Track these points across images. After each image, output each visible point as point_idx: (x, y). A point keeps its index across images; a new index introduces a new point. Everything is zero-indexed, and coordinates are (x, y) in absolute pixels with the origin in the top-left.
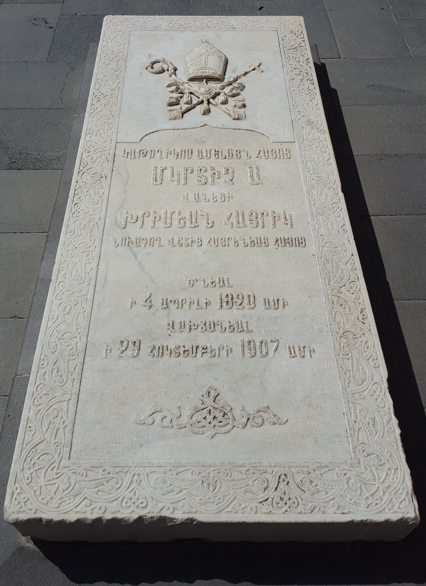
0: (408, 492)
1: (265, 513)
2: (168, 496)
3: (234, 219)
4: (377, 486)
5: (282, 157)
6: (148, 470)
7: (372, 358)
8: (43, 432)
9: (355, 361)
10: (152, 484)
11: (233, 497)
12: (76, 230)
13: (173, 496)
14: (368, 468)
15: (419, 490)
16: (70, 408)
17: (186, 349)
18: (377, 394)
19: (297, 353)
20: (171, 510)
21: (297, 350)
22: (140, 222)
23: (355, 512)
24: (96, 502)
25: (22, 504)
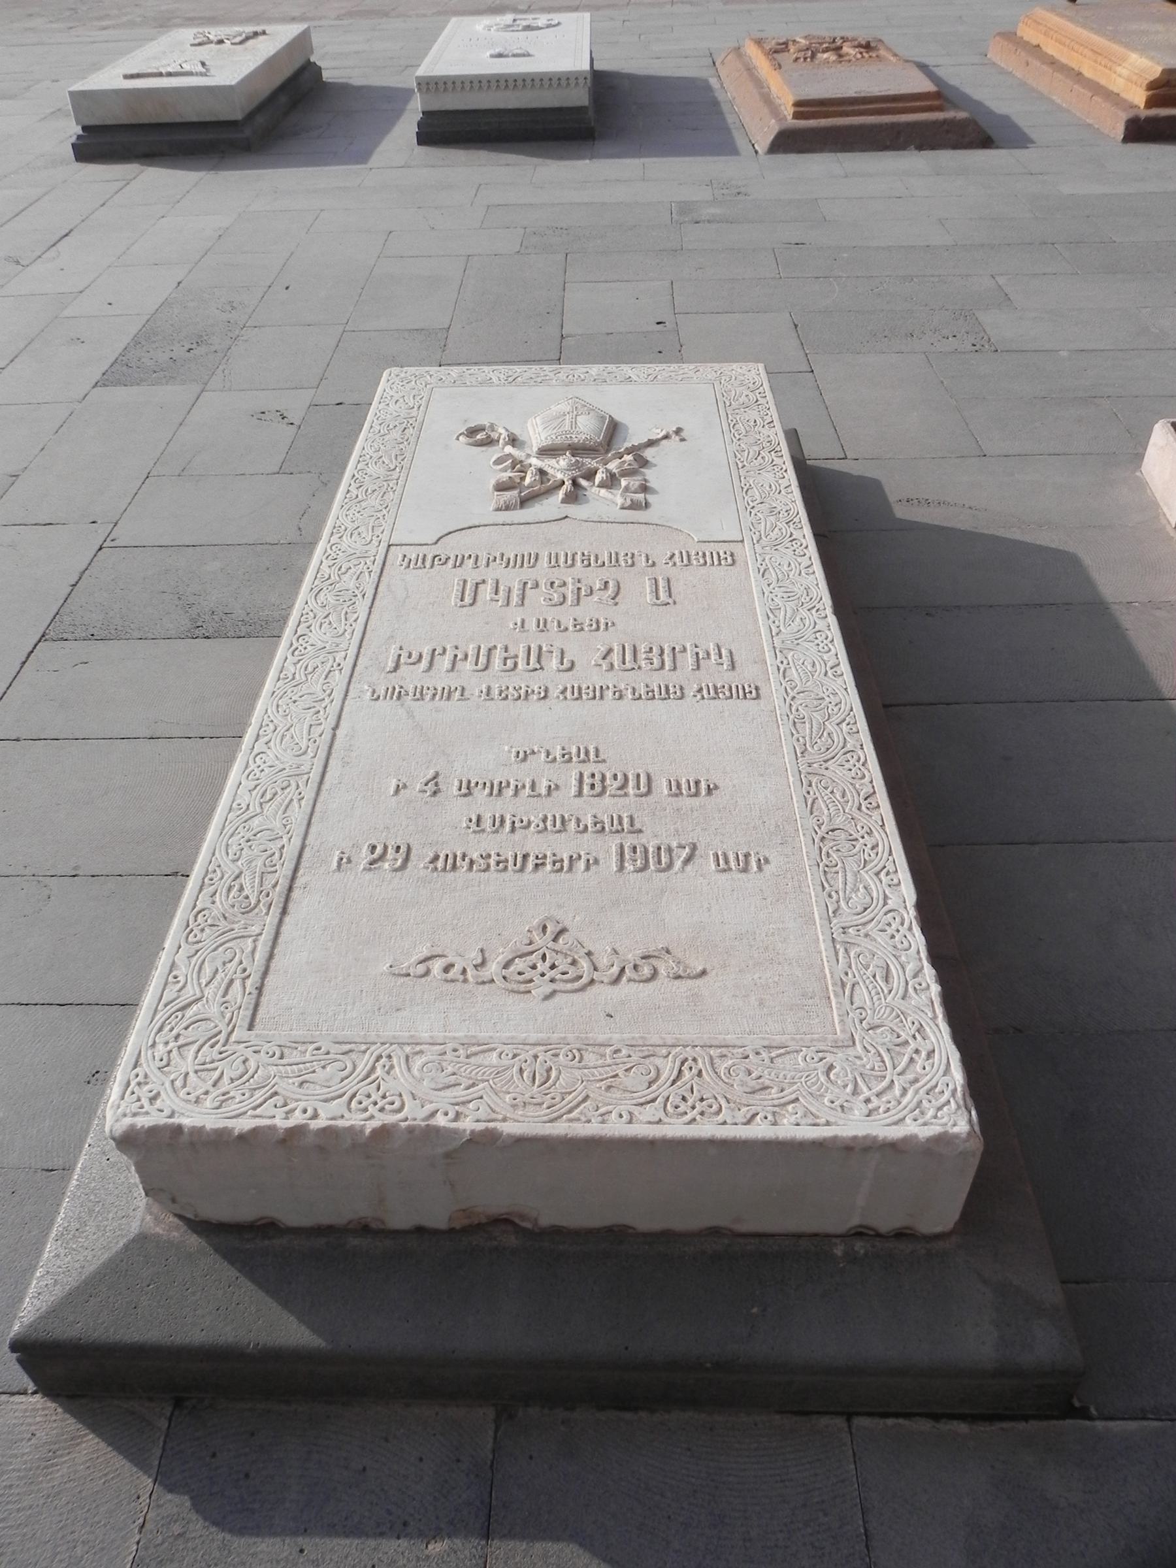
0: (955, 1089)
1: (650, 1123)
2: (448, 1093)
3: (615, 658)
4: (887, 1080)
5: (716, 563)
6: (408, 1049)
7: (885, 870)
8: (200, 984)
9: (849, 875)
10: (415, 1072)
11: (583, 1095)
12: (297, 676)
13: (459, 1093)
14: (870, 1048)
15: (979, 1087)
16: (259, 948)
17: (502, 858)
18: (894, 926)
19: (733, 864)
20: (451, 1115)
21: (732, 858)
22: (424, 663)
23: (841, 1123)
24: (297, 1101)
25: (145, 1102)
